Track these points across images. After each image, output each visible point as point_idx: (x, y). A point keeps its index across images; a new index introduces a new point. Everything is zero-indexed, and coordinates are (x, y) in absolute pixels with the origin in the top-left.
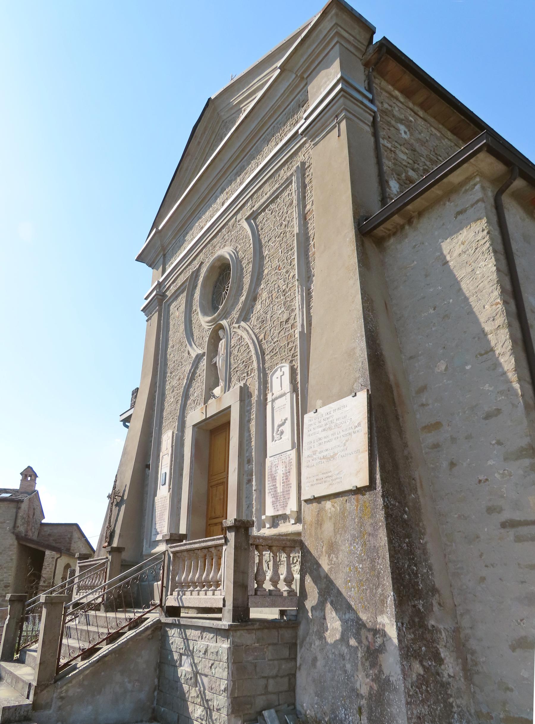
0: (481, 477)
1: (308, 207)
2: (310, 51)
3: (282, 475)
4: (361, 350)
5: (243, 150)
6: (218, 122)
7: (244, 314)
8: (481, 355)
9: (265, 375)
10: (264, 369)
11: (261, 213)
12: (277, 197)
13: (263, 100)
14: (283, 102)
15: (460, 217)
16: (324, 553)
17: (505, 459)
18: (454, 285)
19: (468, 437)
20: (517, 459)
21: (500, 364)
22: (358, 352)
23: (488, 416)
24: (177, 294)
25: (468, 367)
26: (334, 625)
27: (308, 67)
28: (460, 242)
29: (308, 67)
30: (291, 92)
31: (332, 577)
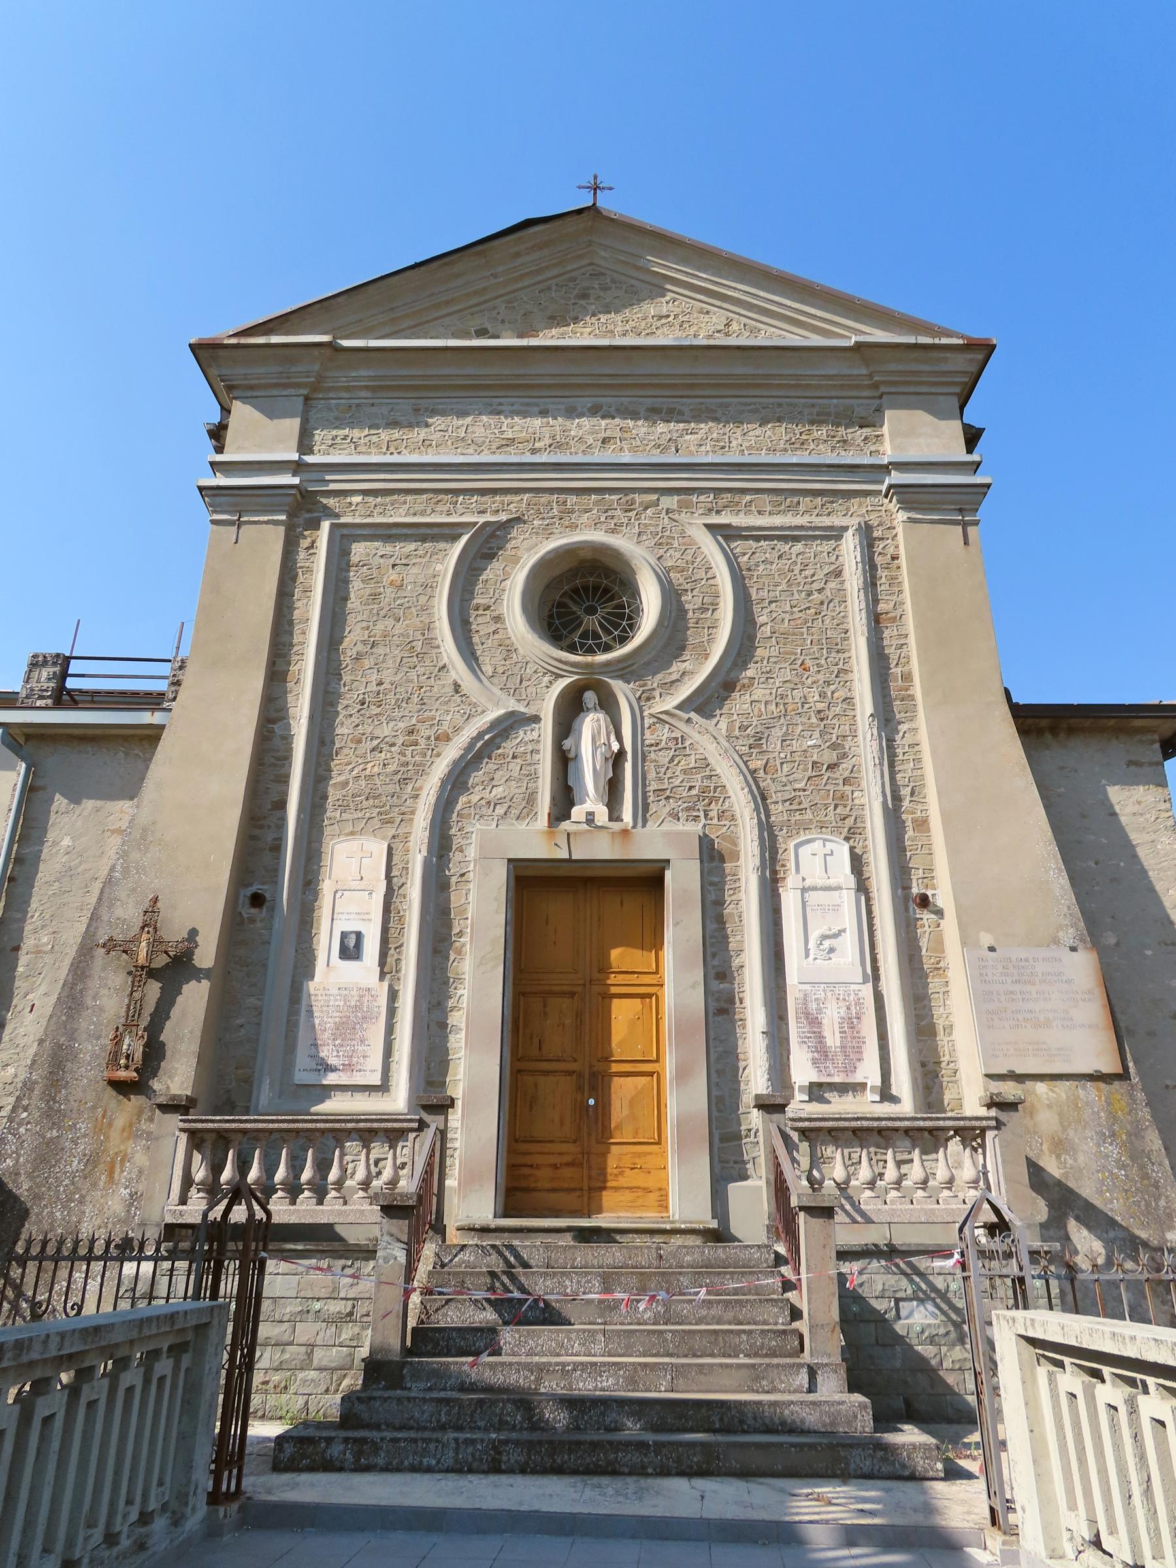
0: (1168, 1082)
1: (882, 607)
3: (837, 1020)
4: (1062, 888)
5: (691, 386)
6: (580, 257)
7: (701, 700)
8: (1166, 944)
9: (773, 838)
10: (770, 827)
11: (746, 538)
12: (796, 539)
13: (789, 354)
14: (819, 387)
15: (1133, 768)
16: (1047, 1153)
22: (1057, 891)
24: (394, 531)
25: (1149, 953)
28: (1134, 799)
30: (842, 387)
31: (1071, 1184)
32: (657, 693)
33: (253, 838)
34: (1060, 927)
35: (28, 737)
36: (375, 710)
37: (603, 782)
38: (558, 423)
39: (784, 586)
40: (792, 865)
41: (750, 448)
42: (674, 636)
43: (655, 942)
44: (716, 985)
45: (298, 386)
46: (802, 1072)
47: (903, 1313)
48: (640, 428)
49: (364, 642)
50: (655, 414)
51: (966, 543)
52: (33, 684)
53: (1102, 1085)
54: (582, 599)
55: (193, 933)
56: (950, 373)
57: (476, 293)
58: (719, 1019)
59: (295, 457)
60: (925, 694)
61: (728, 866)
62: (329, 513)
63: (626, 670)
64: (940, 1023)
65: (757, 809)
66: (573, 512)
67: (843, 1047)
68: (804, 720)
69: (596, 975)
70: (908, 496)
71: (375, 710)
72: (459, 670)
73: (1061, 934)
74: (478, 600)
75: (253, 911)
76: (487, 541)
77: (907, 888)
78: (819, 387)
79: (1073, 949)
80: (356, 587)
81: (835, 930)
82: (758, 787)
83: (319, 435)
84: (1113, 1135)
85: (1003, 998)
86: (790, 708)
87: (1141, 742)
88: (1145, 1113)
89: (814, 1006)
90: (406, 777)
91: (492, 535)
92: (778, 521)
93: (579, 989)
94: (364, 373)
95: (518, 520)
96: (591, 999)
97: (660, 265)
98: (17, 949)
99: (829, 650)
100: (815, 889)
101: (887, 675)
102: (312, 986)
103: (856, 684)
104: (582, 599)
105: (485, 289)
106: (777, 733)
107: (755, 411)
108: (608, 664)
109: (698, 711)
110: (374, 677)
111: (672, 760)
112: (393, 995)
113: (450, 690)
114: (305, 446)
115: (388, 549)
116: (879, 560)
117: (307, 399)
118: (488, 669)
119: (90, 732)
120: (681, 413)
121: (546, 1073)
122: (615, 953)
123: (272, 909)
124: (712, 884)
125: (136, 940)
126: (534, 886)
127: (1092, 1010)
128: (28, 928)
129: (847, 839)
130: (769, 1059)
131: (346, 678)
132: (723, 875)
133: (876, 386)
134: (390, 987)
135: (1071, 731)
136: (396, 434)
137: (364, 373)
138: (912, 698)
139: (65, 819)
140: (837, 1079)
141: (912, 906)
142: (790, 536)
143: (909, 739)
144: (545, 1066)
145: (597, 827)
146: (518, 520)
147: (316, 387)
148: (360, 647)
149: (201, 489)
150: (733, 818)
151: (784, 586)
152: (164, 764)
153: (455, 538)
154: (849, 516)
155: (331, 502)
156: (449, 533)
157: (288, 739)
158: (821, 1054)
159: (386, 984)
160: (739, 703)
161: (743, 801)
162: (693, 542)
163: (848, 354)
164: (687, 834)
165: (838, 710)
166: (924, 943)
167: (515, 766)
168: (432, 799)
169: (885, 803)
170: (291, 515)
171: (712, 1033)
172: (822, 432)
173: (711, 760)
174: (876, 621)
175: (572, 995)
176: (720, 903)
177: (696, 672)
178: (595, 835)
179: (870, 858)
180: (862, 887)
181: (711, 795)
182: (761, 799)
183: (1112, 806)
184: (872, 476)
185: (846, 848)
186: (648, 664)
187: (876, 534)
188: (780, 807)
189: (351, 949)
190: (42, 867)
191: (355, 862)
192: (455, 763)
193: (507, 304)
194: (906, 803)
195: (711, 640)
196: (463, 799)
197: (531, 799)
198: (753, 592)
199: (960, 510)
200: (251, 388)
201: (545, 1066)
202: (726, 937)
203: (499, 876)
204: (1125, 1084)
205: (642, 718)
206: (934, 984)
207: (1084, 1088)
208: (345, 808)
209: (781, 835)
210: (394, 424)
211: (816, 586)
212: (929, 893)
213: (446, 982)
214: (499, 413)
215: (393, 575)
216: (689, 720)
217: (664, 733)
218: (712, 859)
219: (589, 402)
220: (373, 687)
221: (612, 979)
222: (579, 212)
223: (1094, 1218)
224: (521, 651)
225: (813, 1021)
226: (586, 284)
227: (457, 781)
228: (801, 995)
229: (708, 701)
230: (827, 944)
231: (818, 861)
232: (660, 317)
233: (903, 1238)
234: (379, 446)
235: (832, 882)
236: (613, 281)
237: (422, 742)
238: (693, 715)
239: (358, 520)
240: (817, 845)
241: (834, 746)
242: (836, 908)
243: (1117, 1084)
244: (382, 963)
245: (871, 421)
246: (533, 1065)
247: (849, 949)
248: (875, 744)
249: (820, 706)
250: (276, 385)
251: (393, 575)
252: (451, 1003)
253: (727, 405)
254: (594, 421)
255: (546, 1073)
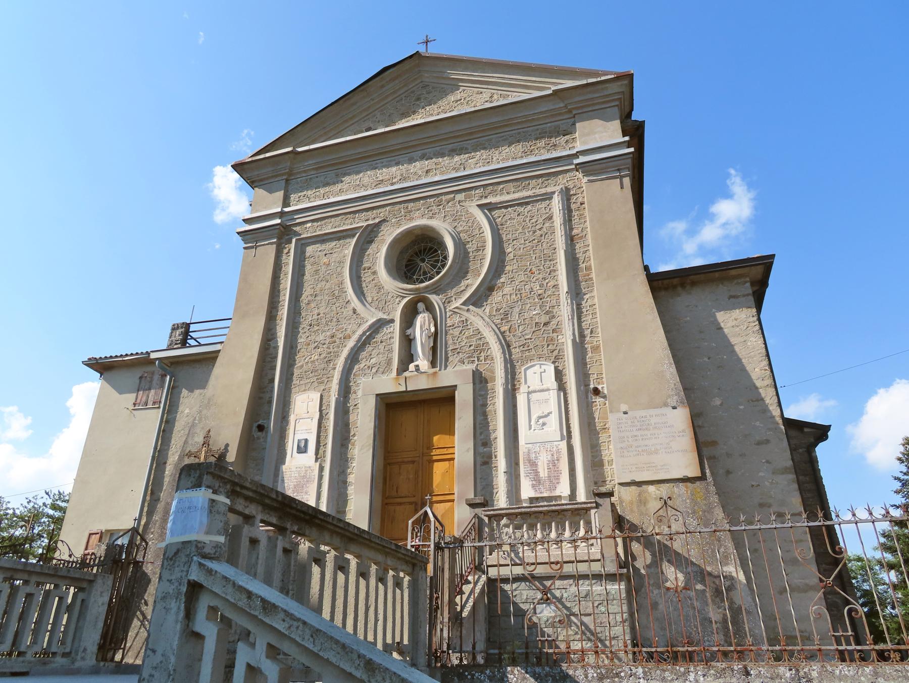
1: (575, 232)
2: (590, 96)
3: (546, 462)
4: (672, 374)
5: (471, 134)
6: (415, 79)
9: (513, 367)
10: (511, 361)
11: (500, 208)
12: (527, 203)
14: (538, 119)
17: (773, 473)
18: (729, 348)
19: (742, 455)
20: (783, 474)
21: (770, 411)
22: (668, 376)
23: (759, 443)
24: (325, 237)
25: (742, 407)
26: (673, 576)
27: (582, 107)
29: (582, 107)
30: (552, 116)
32: (453, 299)
33: (261, 398)
34: (669, 396)
35: (172, 363)
36: (316, 328)
37: (427, 349)
38: (403, 168)
39: (520, 230)
40: (523, 380)
41: (503, 159)
42: (462, 269)
43: (451, 431)
44: (481, 449)
45: (283, 175)
46: (527, 491)
47: (538, 611)
48: (445, 161)
49: (311, 295)
50: (453, 152)
51: (622, 188)
52: (173, 338)
53: (689, 484)
54: (418, 255)
55: (227, 445)
56: (616, 96)
57: (365, 110)
58: (483, 467)
59: (279, 210)
60: (597, 275)
61: (489, 385)
62: (296, 234)
63: (437, 289)
64: (606, 459)
65: (504, 352)
66: (411, 211)
67: (549, 477)
68: (531, 301)
69: (425, 451)
70: (587, 168)
71: (316, 328)
72: (355, 302)
73: (669, 400)
74: (366, 265)
75: (260, 434)
76: (369, 234)
77: (587, 385)
78: (538, 119)
79: (674, 408)
80: (309, 269)
81: (546, 413)
82: (505, 340)
83: (293, 197)
84: (694, 512)
85: (630, 440)
86: (523, 295)
87: (738, 283)
88: (715, 499)
89: (534, 456)
90: (329, 361)
91: (372, 231)
92: (516, 196)
93: (416, 459)
94: (310, 162)
95: (384, 221)
96: (424, 462)
97: (455, 74)
98: (165, 463)
99: (545, 261)
100: (535, 392)
101: (577, 269)
102: (284, 467)
103: (560, 277)
104: (418, 255)
105: (369, 107)
106: (516, 310)
107: (505, 140)
108: (427, 287)
109: (474, 304)
110: (316, 312)
111: (461, 332)
112: (321, 469)
113: (351, 312)
114: (286, 202)
115: (323, 247)
116: (573, 206)
117: (287, 180)
118: (369, 299)
119: (197, 357)
120: (467, 149)
121: (401, 504)
122: (435, 438)
123: (267, 432)
124: (480, 395)
125: (200, 451)
126: (391, 407)
127: (685, 442)
128: (170, 453)
129: (554, 362)
130: (507, 487)
131: (303, 314)
132: (487, 390)
133: (570, 111)
134: (320, 465)
135: (693, 284)
136: (327, 189)
137: (310, 162)
138: (591, 279)
139: (186, 400)
140: (545, 495)
141: (590, 395)
142: (523, 203)
143: (590, 302)
144: (399, 500)
145: (422, 373)
146: (384, 221)
147: (290, 174)
148: (310, 298)
149: (238, 233)
150: (492, 359)
151: (520, 230)
152: (218, 369)
153: (354, 236)
154: (555, 187)
155: (297, 229)
156: (341, 236)
157: (276, 348)
158: (537, 481)
159: (318, 464)
160: (496, 297)
161: (497, 349)
162: (472, 215)
163: (552, 98)
164: (465, 370)
165: (550, 293)
166: (596, 415)
167: (381, 347)
168: (341, 369)
169: (574, 341)
170: (279, 238)
171: (479, 476)
172: (542, 143)
173: (481, 330)
174: (571, 240)
175: (413, 462)
176: (485, 405)
177: (473, 283)
178: (422, 377)
179: (566, 371)
180: (562, 387)
181: (481, 348)
182: (507, 347)
183: (719, 324)
184: (568, 161)
185: (552, 367)
186: (448, 284)
187: (572, 193)
188: (517, 350)
189: (302, 449)
190: (176, 424)
191: (305, 405)
192: (352, 349)
193: (383, 110)
194: (588, 339)
195: (482, 266)
196: (356, 367)
197: (389, 362)
198: (504, 236)
199: (618, 170)
200: (261, 180)
201: (399, 500)
202: (488, 423)
203: (372, 402)
204: (703, 483)
205: (446, 313)
206: (603, 437)
207: (678, 487)
208: (301, 378)
209: (517, 365)
210: (327, 184)
211: (538, 227)
212: (600, 387)
213: (347, 461)
214: (376, 168)
215: (325, 260)
216: (468, 310)
217: (456, 319)
218: (481, 382)
219: (420, 153)
220: (315, 317)
221: (434, 452)
222: (411, 57)
223: (678, 560)
224: (386, 287)
225: (533, 464)
226: (419, 93)
227: (353, 358)
228: (526, 450)
229: (478, 299)
230: (541, 421)
231: (538, 377)
232: (457, 101)
233: (540, 570)
234: (319, 197)
235: (545, 387)
236: (433, 88)
237: (338, 341)
238: (471, 307)
239: (309, 235)
240: (537, 368)
241: (547, 313)
242: (547, 401)
243: (698, 483)
244: (317, 453)
245: (568, 131)
246: (392, 501)
247: (553, 423)
248: (569, 308)
249: (540, 292)
250: (272, 177)
251: (325, 260)
252: (349, 471)
253: (491, 140)
254: (422, 162)
255: (401, 504)
